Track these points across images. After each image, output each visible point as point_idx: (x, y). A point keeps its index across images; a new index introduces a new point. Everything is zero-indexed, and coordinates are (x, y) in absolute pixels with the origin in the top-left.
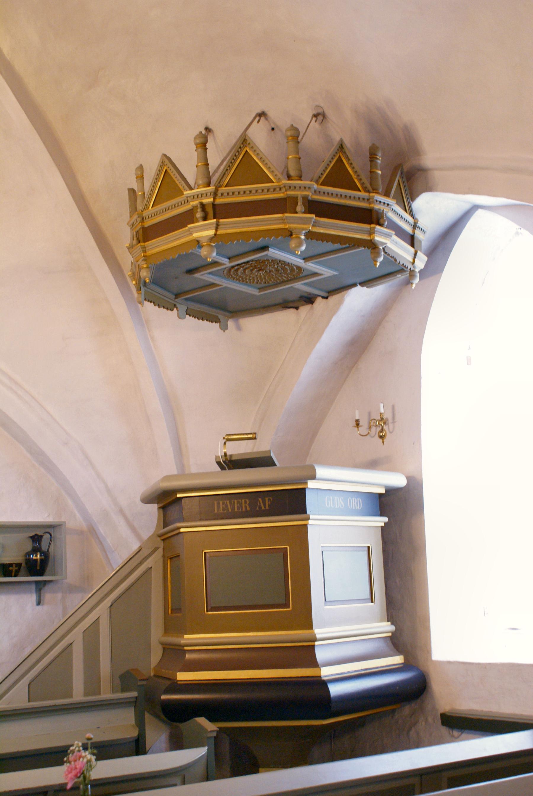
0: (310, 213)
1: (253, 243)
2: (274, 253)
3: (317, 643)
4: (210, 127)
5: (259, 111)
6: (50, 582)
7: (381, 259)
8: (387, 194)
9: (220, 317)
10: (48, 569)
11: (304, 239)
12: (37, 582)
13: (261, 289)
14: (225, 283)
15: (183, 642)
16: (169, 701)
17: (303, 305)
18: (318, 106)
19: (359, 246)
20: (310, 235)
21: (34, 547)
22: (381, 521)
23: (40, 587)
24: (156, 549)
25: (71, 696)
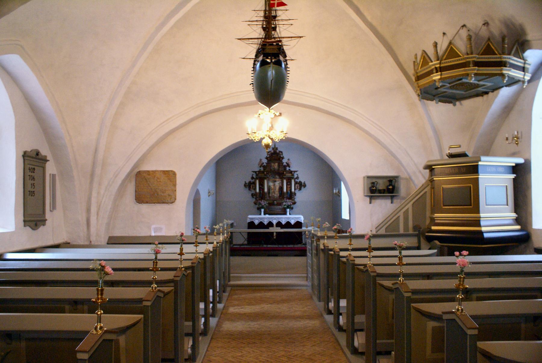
0: (475, 66)
1: (457, 78)
2: (464, 80)
3: (481, 219)
4: (445, 32)
5: (462, 25)
6: (396, 196)
7: (506, 79)
8: (509, 54)
9: (452, 101)
10: (395, 191)
11: (473, 76)
12: (391, 196)
13: (465, 91)
14: (451, 91)
15: (434, 216)
16: (428, 235)
17: (484, 95)
18: (485, 20)
19: (496, 76)
20: (476, 74)
21: (372, 185)
22: (513, 176)
23: (392, 197)
24: (428, 185)
25: (399, 232)
